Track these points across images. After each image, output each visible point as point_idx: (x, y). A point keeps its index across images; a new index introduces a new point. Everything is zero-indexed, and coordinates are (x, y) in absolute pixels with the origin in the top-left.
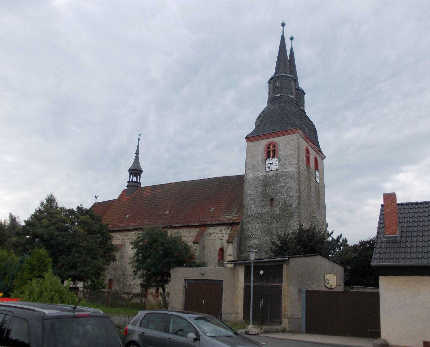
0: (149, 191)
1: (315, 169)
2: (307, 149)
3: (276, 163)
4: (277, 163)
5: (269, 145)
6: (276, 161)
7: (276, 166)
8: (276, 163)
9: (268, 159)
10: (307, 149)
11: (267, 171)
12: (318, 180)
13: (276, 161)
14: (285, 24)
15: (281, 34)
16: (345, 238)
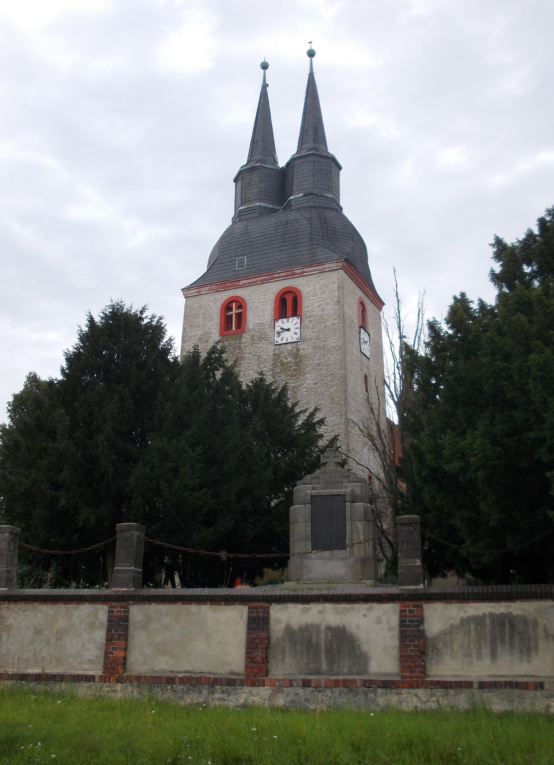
0: (389, 388)
1: (360, 327)
2: (362, 303)
3: (296, 329)
4: (298, 328)
5: (283, 295)
6: (297, 323)
7: (296, 333)
8: (296, 329)
9: (280, 321)
10: (362, 303)
11: (277, 343)
12: (366, 349)
13: (297, 323)
14: (314, 51)
15: (308, 72)
16: (480, 300)
